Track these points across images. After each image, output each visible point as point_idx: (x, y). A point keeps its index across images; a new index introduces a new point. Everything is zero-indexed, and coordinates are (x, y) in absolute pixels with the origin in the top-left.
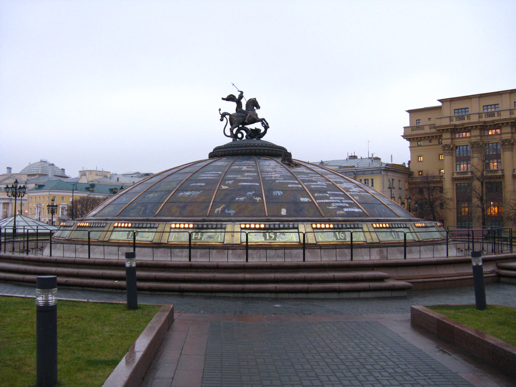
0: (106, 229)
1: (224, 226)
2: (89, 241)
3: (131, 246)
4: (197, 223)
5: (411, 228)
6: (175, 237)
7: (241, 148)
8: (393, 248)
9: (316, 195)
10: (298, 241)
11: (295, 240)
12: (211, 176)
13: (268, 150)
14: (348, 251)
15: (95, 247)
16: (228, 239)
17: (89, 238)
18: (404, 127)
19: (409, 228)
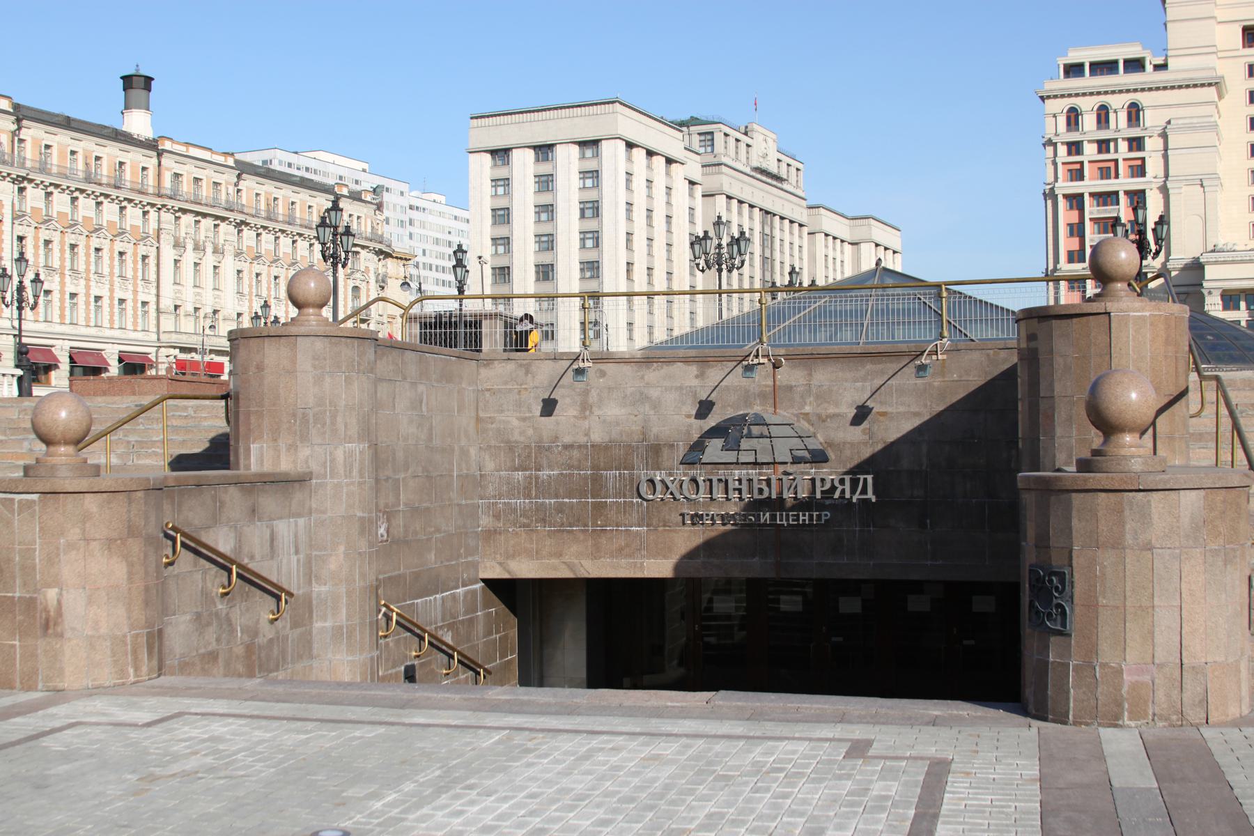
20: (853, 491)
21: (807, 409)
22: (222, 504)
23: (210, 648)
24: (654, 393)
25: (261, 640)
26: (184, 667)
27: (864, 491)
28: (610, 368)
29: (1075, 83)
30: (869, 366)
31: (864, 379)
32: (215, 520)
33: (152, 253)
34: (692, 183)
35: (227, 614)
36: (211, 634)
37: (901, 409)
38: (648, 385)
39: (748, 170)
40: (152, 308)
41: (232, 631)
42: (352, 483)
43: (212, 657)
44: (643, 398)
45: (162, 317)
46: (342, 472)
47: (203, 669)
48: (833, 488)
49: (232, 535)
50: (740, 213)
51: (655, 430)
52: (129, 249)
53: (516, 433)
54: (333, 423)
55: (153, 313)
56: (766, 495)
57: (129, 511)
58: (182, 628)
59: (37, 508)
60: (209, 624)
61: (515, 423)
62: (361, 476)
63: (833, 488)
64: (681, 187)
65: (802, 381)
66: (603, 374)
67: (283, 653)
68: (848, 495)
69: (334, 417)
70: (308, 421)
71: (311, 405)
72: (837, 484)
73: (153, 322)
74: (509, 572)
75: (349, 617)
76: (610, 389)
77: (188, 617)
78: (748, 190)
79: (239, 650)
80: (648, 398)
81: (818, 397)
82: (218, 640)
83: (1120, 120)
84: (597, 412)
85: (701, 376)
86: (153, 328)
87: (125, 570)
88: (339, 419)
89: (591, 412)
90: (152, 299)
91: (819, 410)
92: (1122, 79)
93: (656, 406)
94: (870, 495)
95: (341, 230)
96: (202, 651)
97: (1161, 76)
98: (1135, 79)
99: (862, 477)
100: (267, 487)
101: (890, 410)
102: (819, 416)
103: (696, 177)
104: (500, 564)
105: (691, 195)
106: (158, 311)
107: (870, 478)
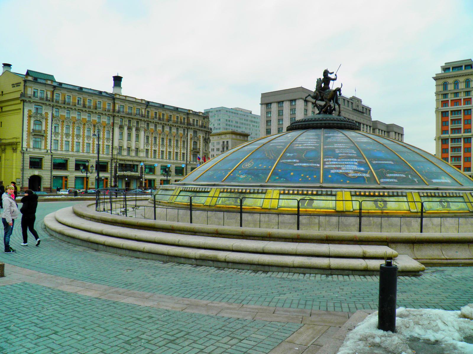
0: (211, 194)
1: (334, 193)
2: (360, 213)
3: (237, 212)
4: (312, 189)
5: (465, 197)
6: (222, 201)
7: (345, 123)
8: (264, 215)
9: (374, 162)
10: (408, 209)
11: (405, 208)
12: (310, 143)
13: (344, 124)
14: (354, 221)
15: (247, 214)
16: (267, 204)
17: (360, 209)
18: (113, 77)
19: (462, 197)
33: (111, 131)
40: (111, 147)
55: (111, 149)
83: (462, 86)
85: (99, 118)
86: (111, 154)
90: (110, 144)
92: (464, 71)
106: (112, 148)
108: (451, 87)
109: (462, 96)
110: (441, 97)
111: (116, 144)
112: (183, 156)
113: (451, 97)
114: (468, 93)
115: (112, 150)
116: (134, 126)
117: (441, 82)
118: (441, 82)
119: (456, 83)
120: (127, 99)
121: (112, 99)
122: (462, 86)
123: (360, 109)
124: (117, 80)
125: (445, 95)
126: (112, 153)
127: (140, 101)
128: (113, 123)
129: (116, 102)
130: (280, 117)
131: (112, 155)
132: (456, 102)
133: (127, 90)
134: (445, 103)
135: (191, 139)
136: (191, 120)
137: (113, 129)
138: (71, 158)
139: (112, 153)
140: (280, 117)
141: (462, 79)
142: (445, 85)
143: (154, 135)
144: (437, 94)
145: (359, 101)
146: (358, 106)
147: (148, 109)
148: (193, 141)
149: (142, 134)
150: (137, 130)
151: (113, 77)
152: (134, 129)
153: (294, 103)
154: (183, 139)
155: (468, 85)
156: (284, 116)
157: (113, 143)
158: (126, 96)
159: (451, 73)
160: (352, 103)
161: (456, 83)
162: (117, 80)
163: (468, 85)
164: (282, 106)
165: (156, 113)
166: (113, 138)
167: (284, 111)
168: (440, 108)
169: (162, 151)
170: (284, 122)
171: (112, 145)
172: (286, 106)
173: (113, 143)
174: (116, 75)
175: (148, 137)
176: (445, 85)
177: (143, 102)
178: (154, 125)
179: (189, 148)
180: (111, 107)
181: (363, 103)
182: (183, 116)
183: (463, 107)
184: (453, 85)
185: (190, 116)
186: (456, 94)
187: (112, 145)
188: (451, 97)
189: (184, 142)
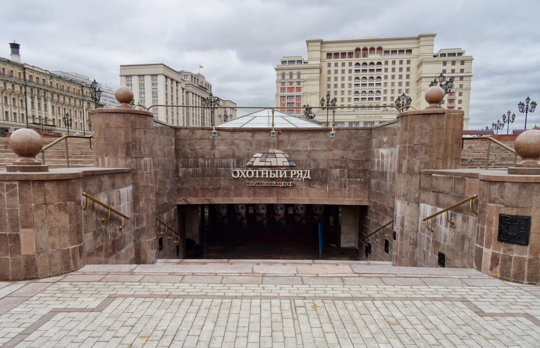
18: (10, 44)
20: (303, 176)
21: (288, 148)
22: (102, 182)
23: (100, 245)
24: (237, 142)
25: (117, 238)
26: (90, 254)
27: (307, 175)
28: (222, 133)
29: (285, 66)
30: (310, 134)
31: (307, 139)
32: (100, 190)
33: (24, 100)
34: (183, 89)
35: (105, 229)
36: (99, 239)
37: (320, 149)
38: (235, 139)
39: (197, 86)
40: (25, 116)
41: (107, 236)
42: (147, 173)
43: (100, 249)
44: (233, 143)
45: (29, 119)
46: (143, 168)
47: (97, 254)
48: (297, 174)
49: (106, 196)
50: (196, 98)
51: (237, 154)
52: (16, 97)
53: (189, 154)
54: (140, 149)
55: (25, 117)
56: (274, 176)
57: (68, 189)
58: (89, 238)
59: (17, 188)
60: (99, 235)
61: (189, 151)
62: (151, 170)
63: (297, 174)
64: (180, 90)
65: (287, 139)
66: (219, 135)
67: (125, 241)
68: (301, 177)
69: (140, 146)
70: (129, 148)
71: (130, 142)
72: (298, 173)
73: (25, 120)
74: (187, 202)
75: (147, 225)
76: (222, 140)
77: (91, 233)
78: (198, 91)
79: (110, 243)
80: (235, 144)
81: (292, 144)
82: (102, 241)
83: (295, 77)
84: (217, 148)
85: (253, 136)
86: (25, 122)
87: (68, 218)
88: (142, 148)
89: (215, 148)
90: (24, 113)
91: (292, 149)
92: (296, 65)
93: (238, 146)
94: (309, 177)
95: (97, 89)
96: (97, 247)
97: (306, 66)
98: (300, 66)
99: (306, 171)
100: (117, 175)
101: (315, 149)
102: (292, 150)
103: (184, 87)
104: (184, 199)
105: (183, 92)
106: (27, 117)
107: (309, 171)
108: (287, 77)
109: (295, 85)
110: (280, 84)
111: (30, 114)
112: (23, 117)
113: (287, 85)
114: (299, 83)
115: (27, 119)
116: (49, 98)
117: (280, 72)
118: (280, 72)
119: (291, 75)
120: (35, 69)
121: (22, 68)
122: (295, 77)
123: (204, 85)
124: (15, 47)
125: (283, 83)
126: (27, 121)
127: (45, 72)
128: (25, 93)
129: (26, 71)
130: (142, 91)
131: (27, 124)
132: (291, 89)
133: (26, 56)
134: (283, 89)
135: (86, 110)
136: (85, 92)
137: (26, 98)
138: (11, 127)
139: (27, 121)
140: (142, 91)
141: (295, 72)
142: (283, 75)
143: (12, 97)
144: (277, 82)
145: (203, 77)
146: (202, 83)
147: (52, 80)
148: (88, 112)
149: (49, 104)
150: (45, 100)
151: (10, 44)
152: (36, 98)
153: (155, 78)
154: (80, 110)
155: (299, 77)
156: (146, 90)
157: (26, 112)
158: (33, 67)
159: (287, 66)
160: (198, 80)
161: (291, 75)
162: (15, 47)
163: (299, 77)
164: (144, 80)
165: (57, 84)
166: (26, 107)
167: (145, 85)
168: (280, 93)
169: (15, 114)
170: (146, 96)
171: (27, 114)
172: (148, 80)
173: (26, 112)
174: (13, 42)
175: (53, 107)
176: (283, 75)
177: (48, 73)
178: (11, 85)
179: (85, 119)
180: (22, 77)
181: (206, 80)
182: (78, 88)
183: (295, 93)
184: (289, 76)
185: (84, 89)
186: (291, 83)
187: (27, 114)
188: (287, 85)
189: (22, 101)
